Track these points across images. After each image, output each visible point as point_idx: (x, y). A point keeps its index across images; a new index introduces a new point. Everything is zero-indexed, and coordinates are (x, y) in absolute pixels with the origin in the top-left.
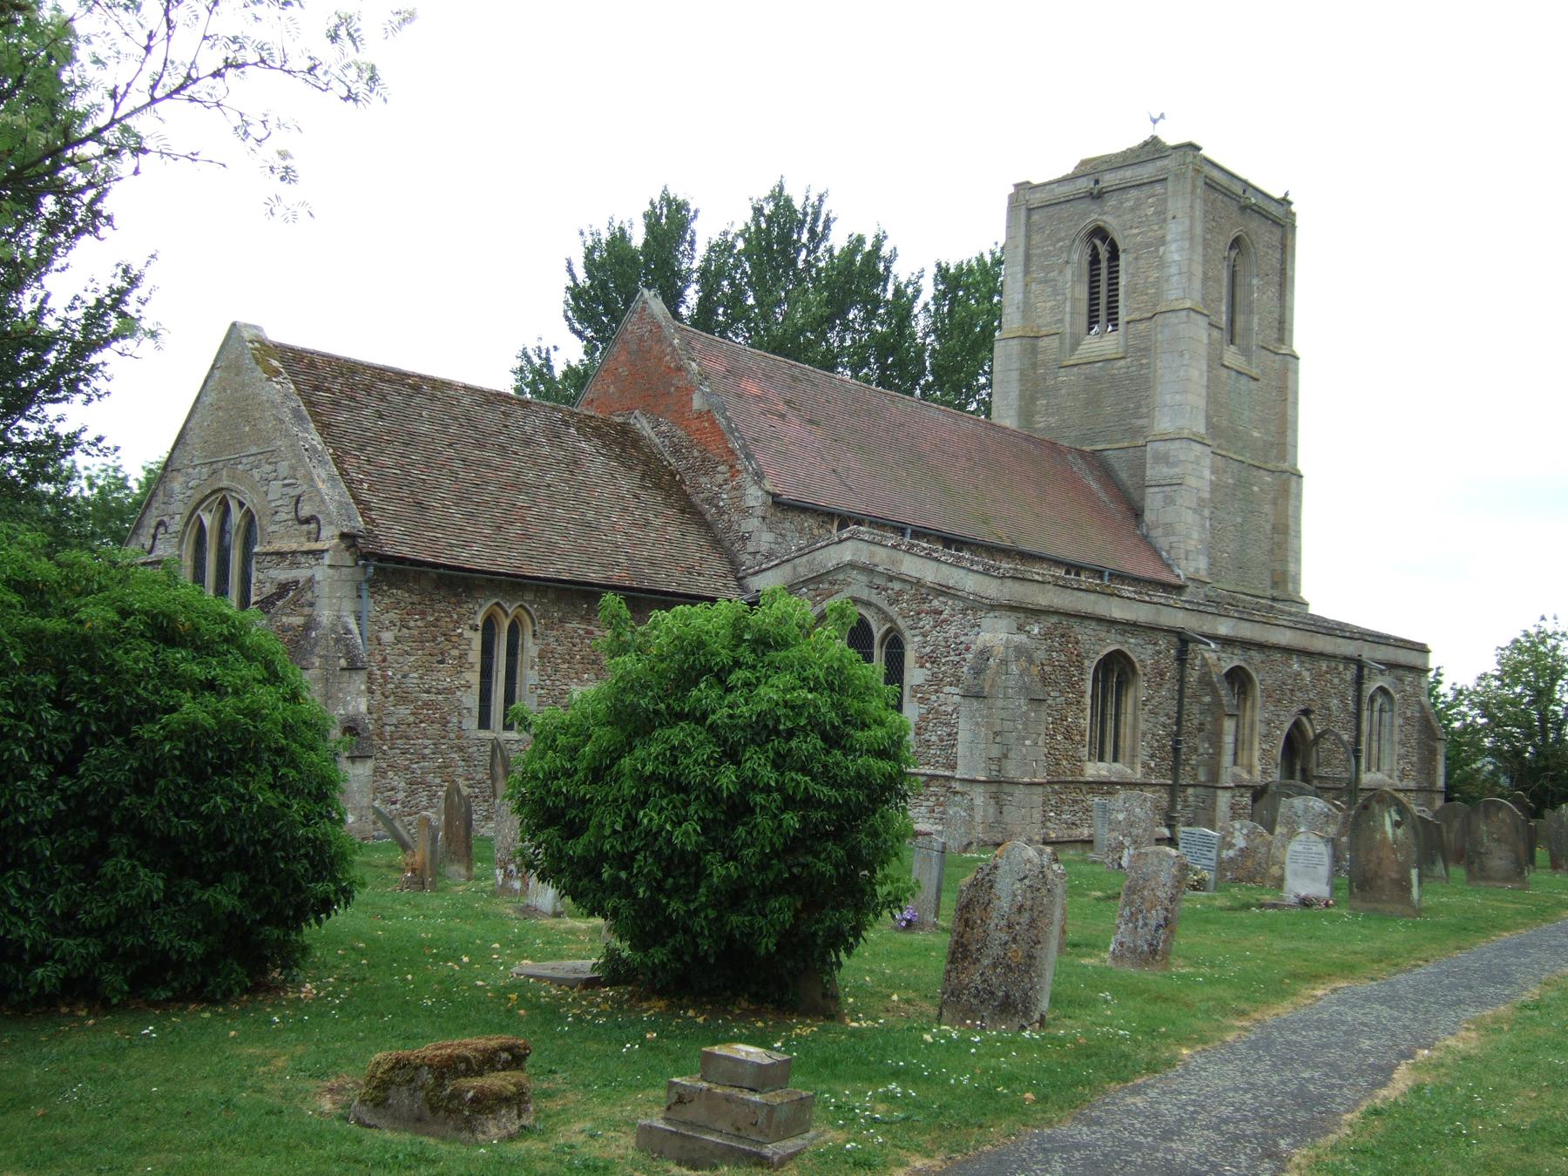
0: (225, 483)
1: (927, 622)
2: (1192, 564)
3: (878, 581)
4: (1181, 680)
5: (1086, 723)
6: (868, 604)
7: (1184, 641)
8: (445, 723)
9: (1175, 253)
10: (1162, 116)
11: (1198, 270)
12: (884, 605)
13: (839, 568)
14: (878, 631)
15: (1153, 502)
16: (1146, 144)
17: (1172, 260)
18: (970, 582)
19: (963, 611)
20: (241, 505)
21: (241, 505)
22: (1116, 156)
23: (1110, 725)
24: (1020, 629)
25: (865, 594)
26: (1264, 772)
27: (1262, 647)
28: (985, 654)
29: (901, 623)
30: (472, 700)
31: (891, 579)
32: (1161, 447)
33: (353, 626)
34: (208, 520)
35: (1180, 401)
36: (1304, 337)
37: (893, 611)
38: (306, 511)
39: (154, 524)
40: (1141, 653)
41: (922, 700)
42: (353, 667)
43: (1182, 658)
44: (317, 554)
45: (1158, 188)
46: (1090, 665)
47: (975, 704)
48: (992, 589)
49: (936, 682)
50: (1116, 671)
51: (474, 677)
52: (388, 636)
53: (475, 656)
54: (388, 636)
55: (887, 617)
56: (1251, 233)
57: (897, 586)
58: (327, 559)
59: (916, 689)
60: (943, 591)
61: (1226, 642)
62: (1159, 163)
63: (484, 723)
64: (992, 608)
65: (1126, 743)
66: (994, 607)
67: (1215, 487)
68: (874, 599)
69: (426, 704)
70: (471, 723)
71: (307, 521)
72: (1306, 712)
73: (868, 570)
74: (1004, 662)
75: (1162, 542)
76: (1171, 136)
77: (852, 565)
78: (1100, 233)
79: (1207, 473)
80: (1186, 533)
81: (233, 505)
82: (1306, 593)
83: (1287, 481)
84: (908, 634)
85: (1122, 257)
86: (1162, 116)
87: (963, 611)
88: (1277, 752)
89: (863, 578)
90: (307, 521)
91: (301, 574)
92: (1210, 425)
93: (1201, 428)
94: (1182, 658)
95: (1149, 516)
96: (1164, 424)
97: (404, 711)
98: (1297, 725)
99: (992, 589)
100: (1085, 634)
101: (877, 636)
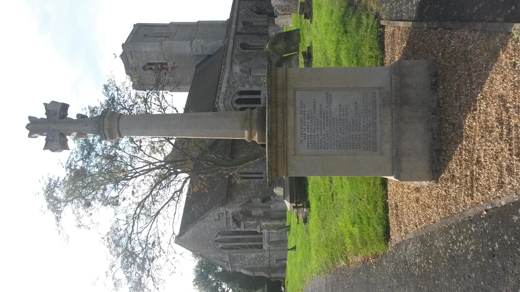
0: (211, 241)
1: (236, 85)
2: (221, 43)
3: (227, 97)
4: (245, 34)
5: (255, 51)
6: (232, 100)
7: (237, 33)
8: (262, 185)
9: (148, 49)
10: (114, 54)
11: (152, 43)
12: (232, 95)
13: (224, 107)
14: (238, 97)
15: (207, 53)
16: (122, 58)
17: (152, 50)
18: (226, 75)
19: (233, 76)
20: (216, 236)
21: (216, 236)
22: (125, 65)
23: (255, 47)
24: (236, 64)
25: (230, 100)
26: (265, 18)
27: (237, 19)
28: (241, 70)
29: (236, 91)
30: (257, 181)
31: (226, 94)
32: (194, 51)
33: (242, 203)
34: (220, 246)
35: (184, 47)
36: (166, 21)
37: (233, 93)
38: (217, 217)
39: (221, 262)
40: (240, 41)
41: (252, 86)
42: (250, 201)
43: (240, 34)
44: (227, 212)
45: (133, 53)
46: (243, 51)
47: (252, 72)
48: (227, 71)
49: (248, 82)
50: (244, 46)
51: (252, 180)
52: (244, 197)
53: (247, 180)
54: (244, 197)
55: (235, 95)
56: (142, 33)
57: (228, 93)
58: (227, 210)
59: (250, 87)
60: (228, 82)
61: (237, 25)
62: (127, 53)
63: (262, 178)
64: (232, 70)
65: (260, 44)
66: (231, 69)
67: (202, 39)
68: (231, 98)
69: (258, 189)
70: (262, 180)
71: (219, 217)
72: (251, 10)
73: (225, 99)
74: (243, 66)
75: (216, 50)
76: (120, 51)
77: (224, 104)
78: (144, 68)
79: (200, 40)
80: (213, 45)
81: (217, 239)
82: (225, 19)
83: (200, 25)
84: (238, 89)
85: (150, 62)
86: (114, 54)
87: (233, 76)
88: (261, 16)
89: (227, 101)
90: (219, 217)
91: (231, 216)
92: (188, 40)
93: (189, 42)
94: (240, 34)
95: (210, 54)
96: (188, 50)
97: (260, 193)
98: (255, 12)
99: (227, 71)
100: (236, 52)
101: (239, 97)
